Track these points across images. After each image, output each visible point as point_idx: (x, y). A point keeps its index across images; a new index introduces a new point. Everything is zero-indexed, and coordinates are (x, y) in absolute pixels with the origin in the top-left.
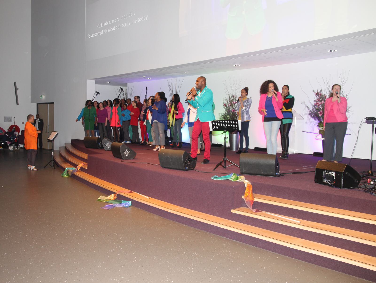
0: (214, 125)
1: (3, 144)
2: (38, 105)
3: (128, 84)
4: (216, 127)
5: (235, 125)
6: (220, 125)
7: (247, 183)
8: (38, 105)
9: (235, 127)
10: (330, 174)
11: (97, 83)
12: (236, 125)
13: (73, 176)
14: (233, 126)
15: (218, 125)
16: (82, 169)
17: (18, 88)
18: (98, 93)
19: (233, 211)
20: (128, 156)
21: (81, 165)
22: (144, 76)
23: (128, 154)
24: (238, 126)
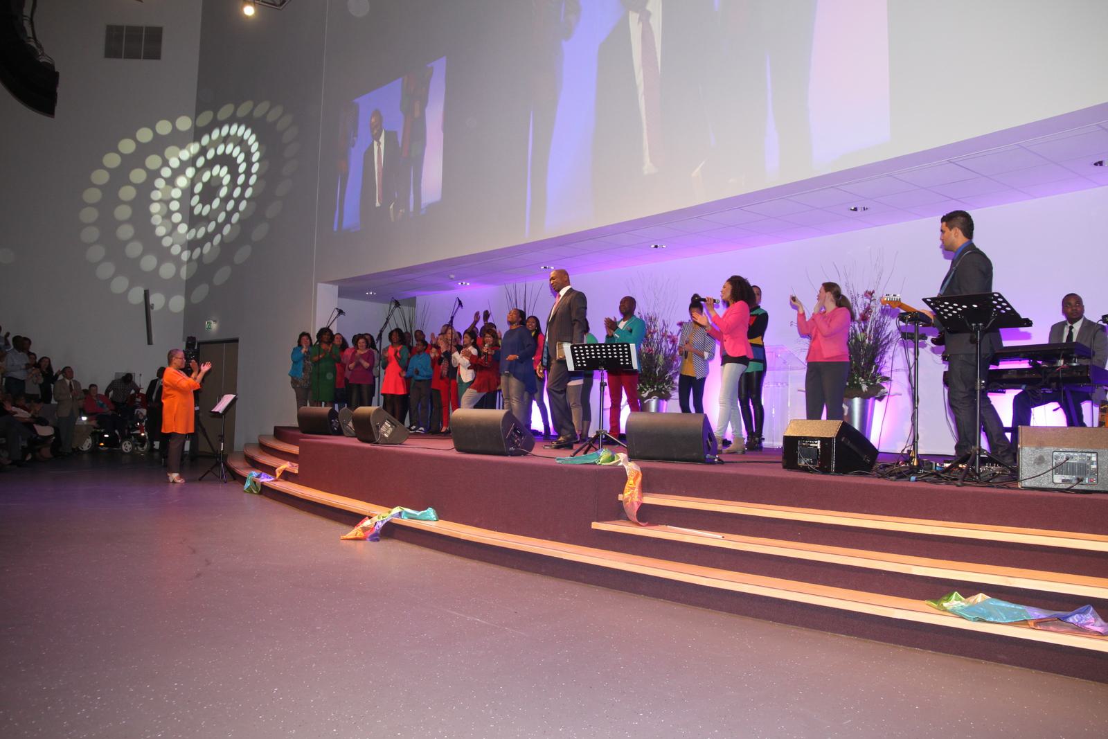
0: (576, 351)
1: (106, 436)
2: (201, 346)
3: (417, 297)
4: (581, 360)
5: (624, 355)
6: (591, 355)
7: (632, 468)
8: (201, 346)
9: (624, 362)
10: (811, 445)
11: (342, 294)
12: (627, 356)
13: (265, 491)
14: (619, 358)
15: (585, 356)
16: (286, 476)
17: (153, 304)
18: (341, 312)
19: (596, 525)
20: (390, 436)
21: (285, 465)
22: (452, 276)
23: (389, 432)
24: (630, 358)
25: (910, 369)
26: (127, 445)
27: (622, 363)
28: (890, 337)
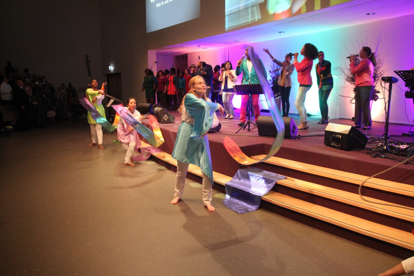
23: (167, 118)
25: (385, 104)
26: (84, 115)
27: (258, 92)
28: (382, 73)
